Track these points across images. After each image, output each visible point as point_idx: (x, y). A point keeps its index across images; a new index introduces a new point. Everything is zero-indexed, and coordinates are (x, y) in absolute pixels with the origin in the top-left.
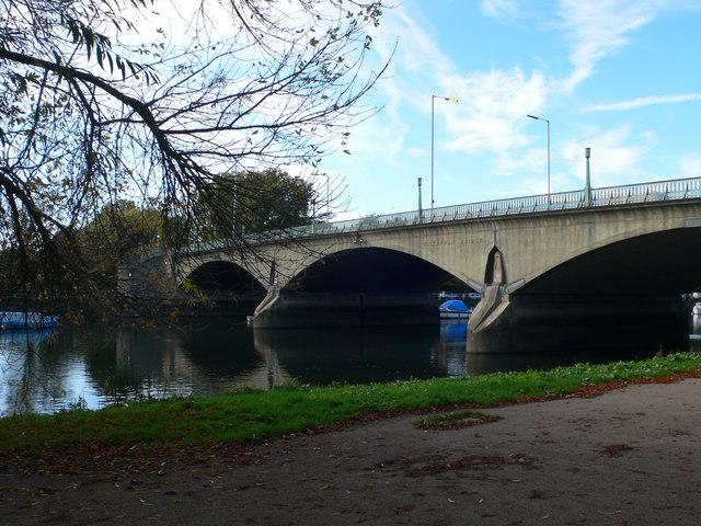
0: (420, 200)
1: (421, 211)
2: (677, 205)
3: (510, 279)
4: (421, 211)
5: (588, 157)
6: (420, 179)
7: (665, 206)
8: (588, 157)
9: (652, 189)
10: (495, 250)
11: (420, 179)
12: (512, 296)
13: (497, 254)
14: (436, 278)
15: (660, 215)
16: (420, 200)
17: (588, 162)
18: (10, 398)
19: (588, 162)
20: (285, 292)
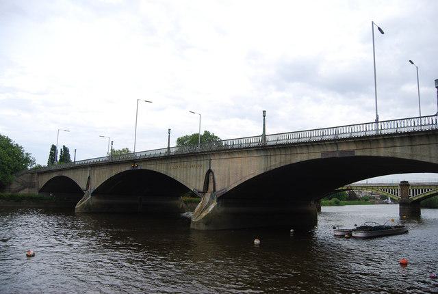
0: (264, 125)
1: (169, 148)
2: (419, 136)
3: (218, 189)
4: (264, 136)
5: (264, 116)
6: (264, 112)
7: (321, 143)
8: (264, 116)
9: (280, 137)
10: (210, 171)
11: (264, 112)
12: (219, 199)
13: (211, 174)
14: (178, 189)
15: (305, 150)
16: (264, 125)
17: (264, 119)
18: (10, 140)
19: (264, 119)
20: (95, 193)
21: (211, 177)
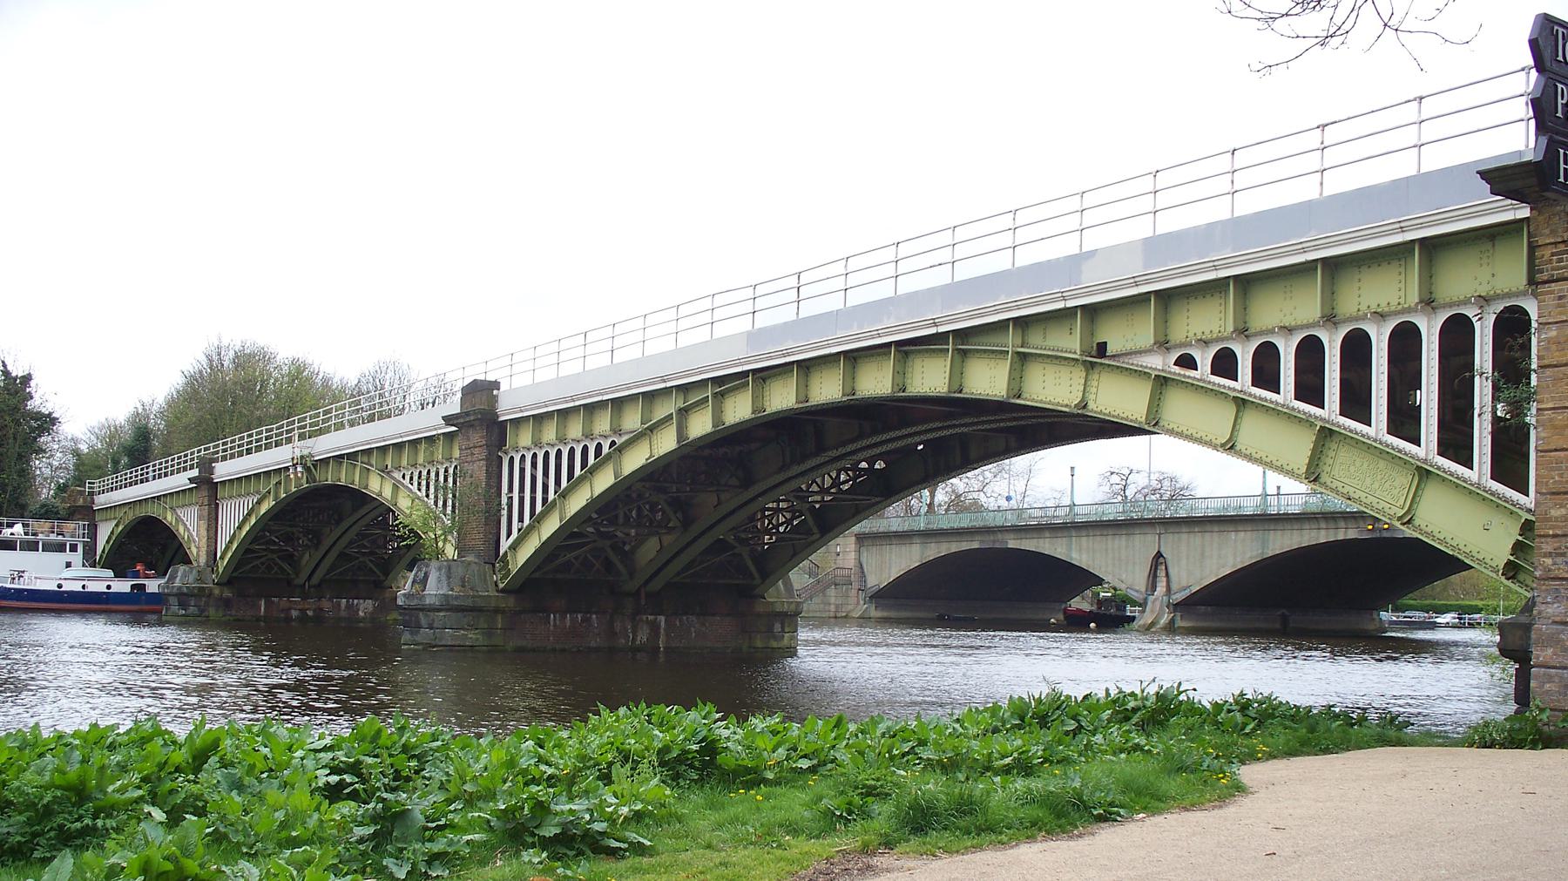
3: (1174, 587)
5: (1073, 476)
8: (1073, 476)
10: (1159, 555)
13: (1161, 560)
17: (1072, 480)
19: (1072, 480)
21: (1161, 573)
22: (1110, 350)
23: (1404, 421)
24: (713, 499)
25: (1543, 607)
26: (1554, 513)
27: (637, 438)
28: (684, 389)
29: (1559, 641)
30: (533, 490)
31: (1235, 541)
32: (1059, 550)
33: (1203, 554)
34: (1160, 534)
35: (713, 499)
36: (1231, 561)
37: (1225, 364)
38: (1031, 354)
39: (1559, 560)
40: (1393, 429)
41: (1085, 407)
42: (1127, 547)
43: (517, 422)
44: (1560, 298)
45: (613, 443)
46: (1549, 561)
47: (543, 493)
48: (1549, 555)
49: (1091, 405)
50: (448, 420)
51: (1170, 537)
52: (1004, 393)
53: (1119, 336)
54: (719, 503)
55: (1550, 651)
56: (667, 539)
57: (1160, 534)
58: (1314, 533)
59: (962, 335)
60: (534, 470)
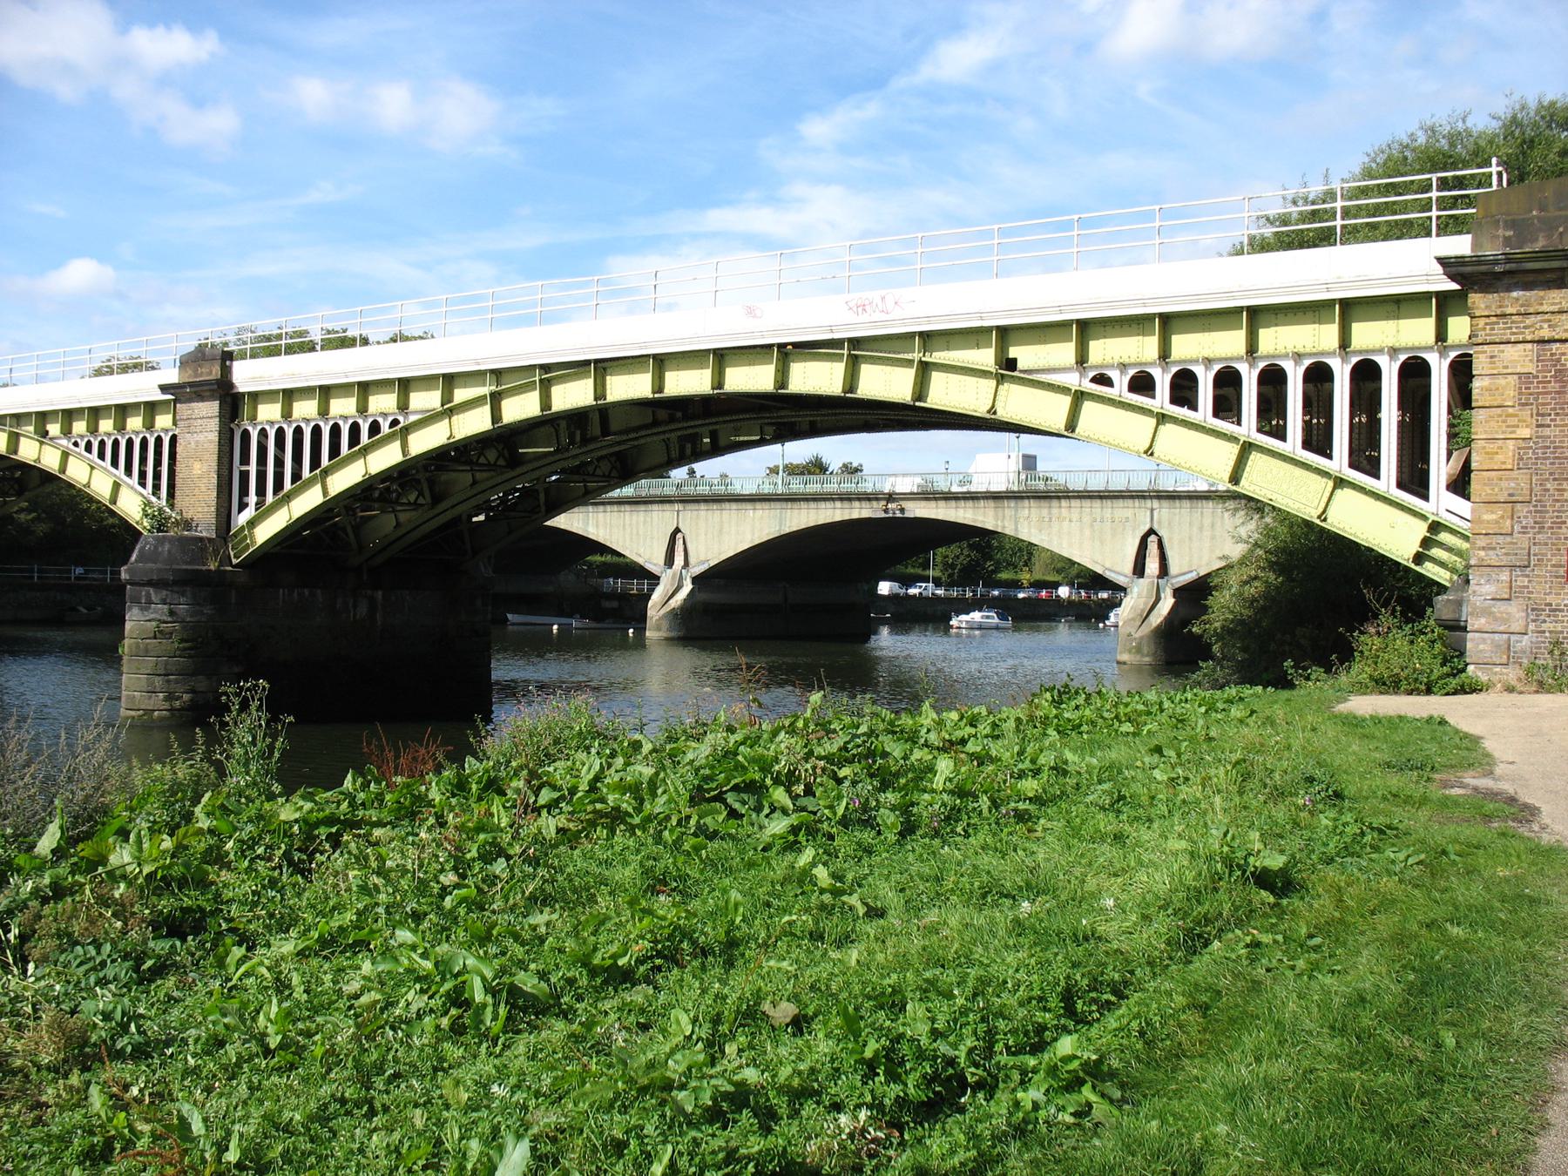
10: (677, 530)
22: (1020, 365)
23: (1318, 440)
24: (468, 478)
25: (1477, 588)
26: (1486, 517)
27: (430, 419)
28: (498, 374)
29: (1491, 613)
30: (158, 463)
31: (754, 519)
32: (576, 524)
33: (721, 531)
34: (678, 511)
35: (468, 478)
36: (749, 537)
37: (1142, 384)
38: (863, 356)
39: (1491, 552)
40: (1307, 445)
41: (995, 413)
42: (645, 522)
43: (256, 397)
44: (1492, 357)
45: (395, 423)
46: (1482, 553)
47: (258, 464)
48: (1483, 548)
49: (999, 413)
50: (164, 388)
51: (688, 514)
52: (840, 390)
53: (1026, 355)
54: (475, 483)
55: (1483, 621)
56: (403, 517)
57: (678, 511)
58: (829, 512)
59: (855, 343)
60: (263, 439)
